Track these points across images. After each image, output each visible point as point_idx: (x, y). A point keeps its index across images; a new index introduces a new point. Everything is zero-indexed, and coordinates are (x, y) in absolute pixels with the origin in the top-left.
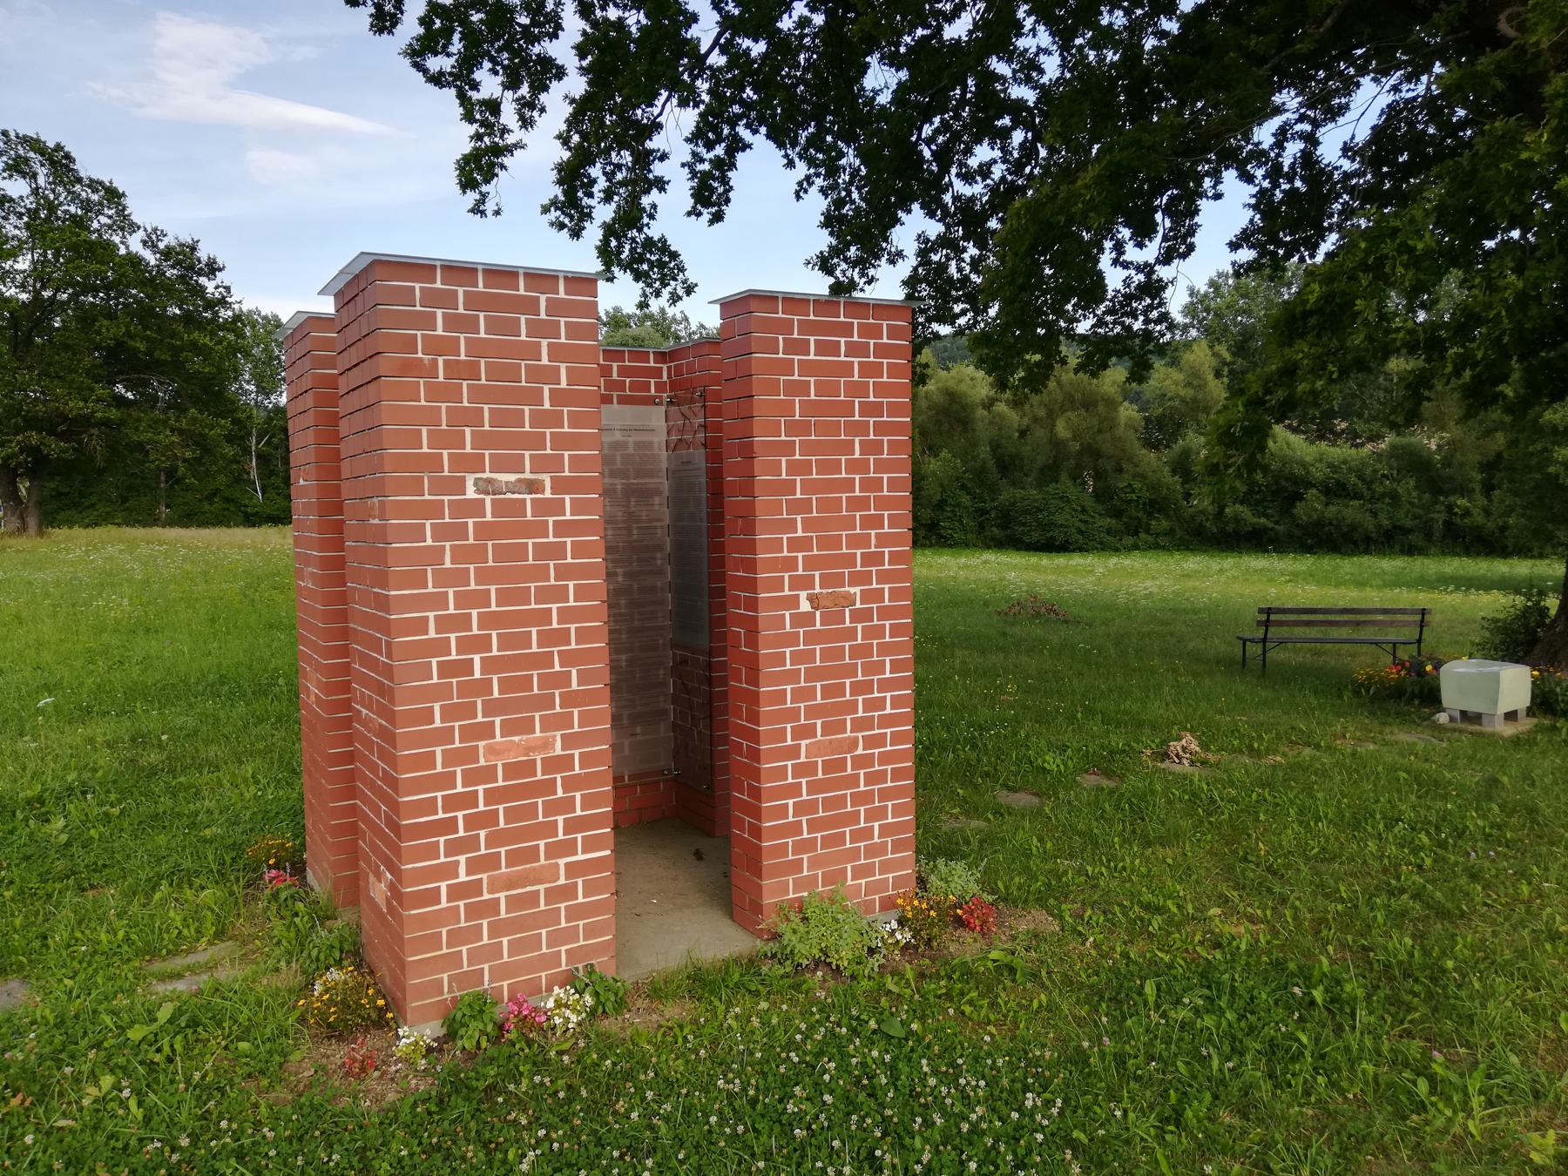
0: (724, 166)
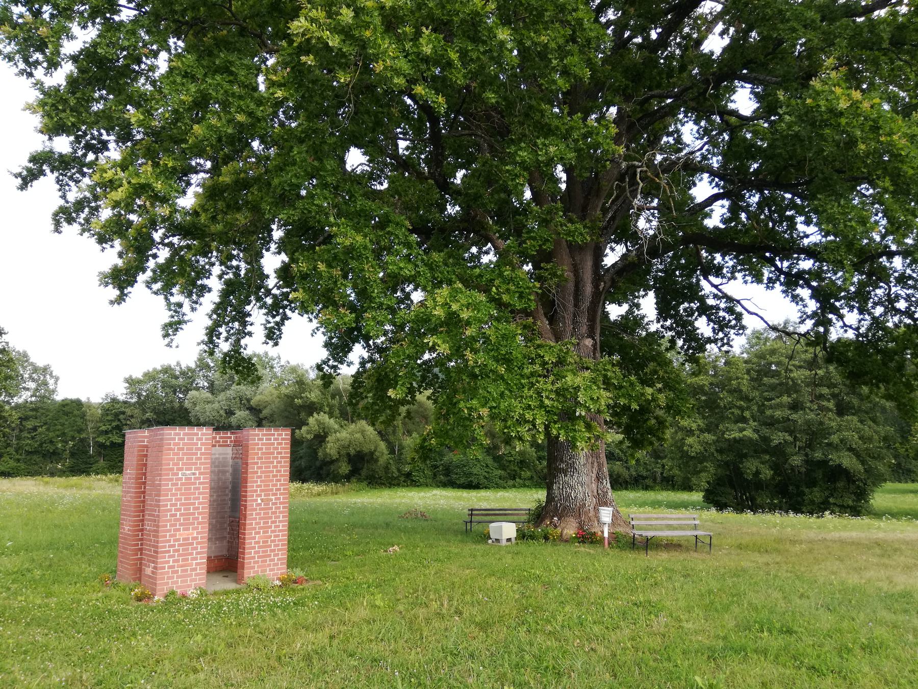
0: (279, 325)
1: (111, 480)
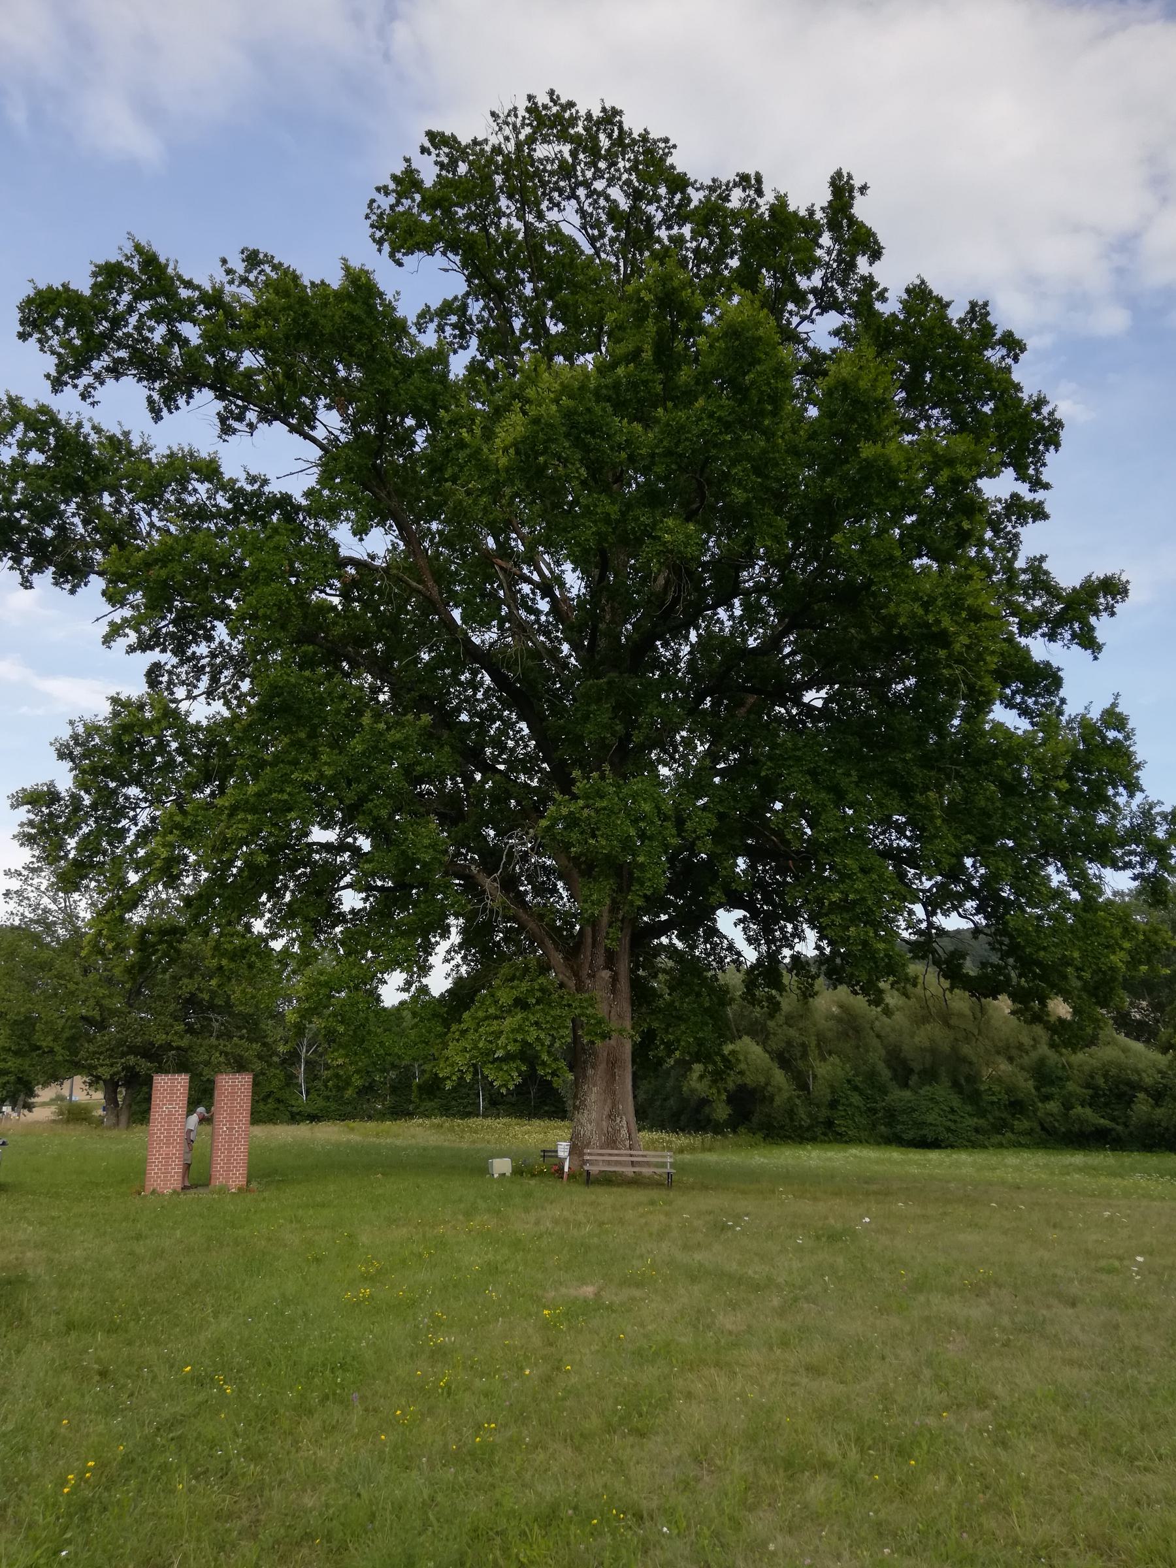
1: (433, 1126)
